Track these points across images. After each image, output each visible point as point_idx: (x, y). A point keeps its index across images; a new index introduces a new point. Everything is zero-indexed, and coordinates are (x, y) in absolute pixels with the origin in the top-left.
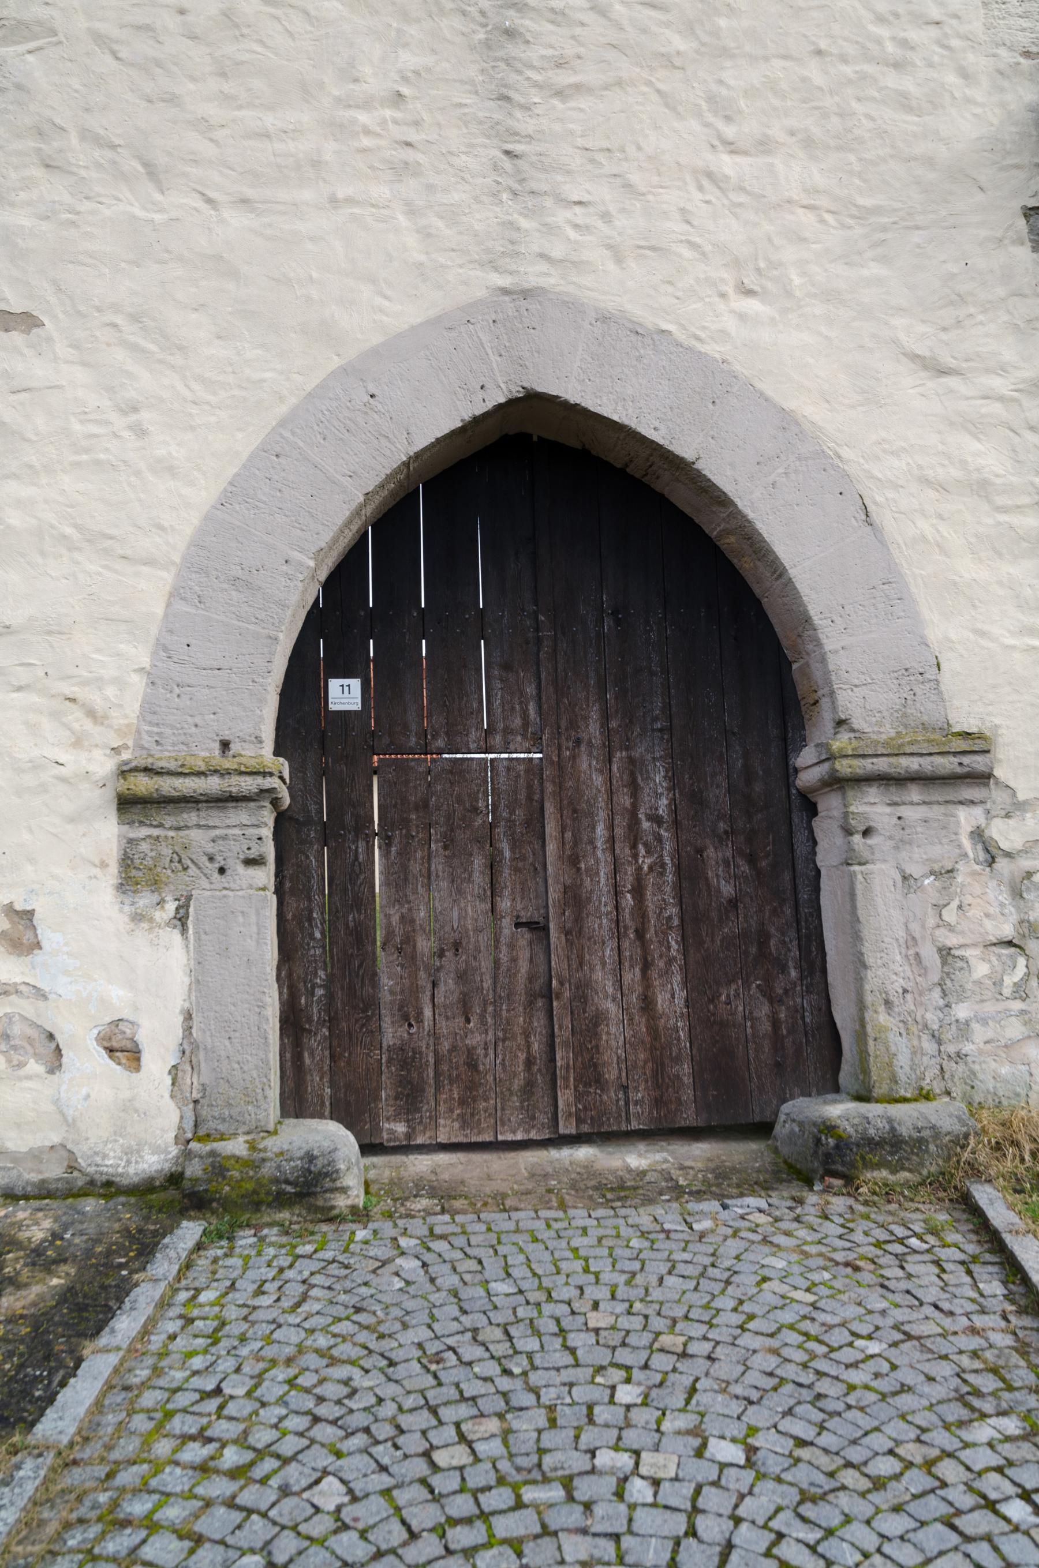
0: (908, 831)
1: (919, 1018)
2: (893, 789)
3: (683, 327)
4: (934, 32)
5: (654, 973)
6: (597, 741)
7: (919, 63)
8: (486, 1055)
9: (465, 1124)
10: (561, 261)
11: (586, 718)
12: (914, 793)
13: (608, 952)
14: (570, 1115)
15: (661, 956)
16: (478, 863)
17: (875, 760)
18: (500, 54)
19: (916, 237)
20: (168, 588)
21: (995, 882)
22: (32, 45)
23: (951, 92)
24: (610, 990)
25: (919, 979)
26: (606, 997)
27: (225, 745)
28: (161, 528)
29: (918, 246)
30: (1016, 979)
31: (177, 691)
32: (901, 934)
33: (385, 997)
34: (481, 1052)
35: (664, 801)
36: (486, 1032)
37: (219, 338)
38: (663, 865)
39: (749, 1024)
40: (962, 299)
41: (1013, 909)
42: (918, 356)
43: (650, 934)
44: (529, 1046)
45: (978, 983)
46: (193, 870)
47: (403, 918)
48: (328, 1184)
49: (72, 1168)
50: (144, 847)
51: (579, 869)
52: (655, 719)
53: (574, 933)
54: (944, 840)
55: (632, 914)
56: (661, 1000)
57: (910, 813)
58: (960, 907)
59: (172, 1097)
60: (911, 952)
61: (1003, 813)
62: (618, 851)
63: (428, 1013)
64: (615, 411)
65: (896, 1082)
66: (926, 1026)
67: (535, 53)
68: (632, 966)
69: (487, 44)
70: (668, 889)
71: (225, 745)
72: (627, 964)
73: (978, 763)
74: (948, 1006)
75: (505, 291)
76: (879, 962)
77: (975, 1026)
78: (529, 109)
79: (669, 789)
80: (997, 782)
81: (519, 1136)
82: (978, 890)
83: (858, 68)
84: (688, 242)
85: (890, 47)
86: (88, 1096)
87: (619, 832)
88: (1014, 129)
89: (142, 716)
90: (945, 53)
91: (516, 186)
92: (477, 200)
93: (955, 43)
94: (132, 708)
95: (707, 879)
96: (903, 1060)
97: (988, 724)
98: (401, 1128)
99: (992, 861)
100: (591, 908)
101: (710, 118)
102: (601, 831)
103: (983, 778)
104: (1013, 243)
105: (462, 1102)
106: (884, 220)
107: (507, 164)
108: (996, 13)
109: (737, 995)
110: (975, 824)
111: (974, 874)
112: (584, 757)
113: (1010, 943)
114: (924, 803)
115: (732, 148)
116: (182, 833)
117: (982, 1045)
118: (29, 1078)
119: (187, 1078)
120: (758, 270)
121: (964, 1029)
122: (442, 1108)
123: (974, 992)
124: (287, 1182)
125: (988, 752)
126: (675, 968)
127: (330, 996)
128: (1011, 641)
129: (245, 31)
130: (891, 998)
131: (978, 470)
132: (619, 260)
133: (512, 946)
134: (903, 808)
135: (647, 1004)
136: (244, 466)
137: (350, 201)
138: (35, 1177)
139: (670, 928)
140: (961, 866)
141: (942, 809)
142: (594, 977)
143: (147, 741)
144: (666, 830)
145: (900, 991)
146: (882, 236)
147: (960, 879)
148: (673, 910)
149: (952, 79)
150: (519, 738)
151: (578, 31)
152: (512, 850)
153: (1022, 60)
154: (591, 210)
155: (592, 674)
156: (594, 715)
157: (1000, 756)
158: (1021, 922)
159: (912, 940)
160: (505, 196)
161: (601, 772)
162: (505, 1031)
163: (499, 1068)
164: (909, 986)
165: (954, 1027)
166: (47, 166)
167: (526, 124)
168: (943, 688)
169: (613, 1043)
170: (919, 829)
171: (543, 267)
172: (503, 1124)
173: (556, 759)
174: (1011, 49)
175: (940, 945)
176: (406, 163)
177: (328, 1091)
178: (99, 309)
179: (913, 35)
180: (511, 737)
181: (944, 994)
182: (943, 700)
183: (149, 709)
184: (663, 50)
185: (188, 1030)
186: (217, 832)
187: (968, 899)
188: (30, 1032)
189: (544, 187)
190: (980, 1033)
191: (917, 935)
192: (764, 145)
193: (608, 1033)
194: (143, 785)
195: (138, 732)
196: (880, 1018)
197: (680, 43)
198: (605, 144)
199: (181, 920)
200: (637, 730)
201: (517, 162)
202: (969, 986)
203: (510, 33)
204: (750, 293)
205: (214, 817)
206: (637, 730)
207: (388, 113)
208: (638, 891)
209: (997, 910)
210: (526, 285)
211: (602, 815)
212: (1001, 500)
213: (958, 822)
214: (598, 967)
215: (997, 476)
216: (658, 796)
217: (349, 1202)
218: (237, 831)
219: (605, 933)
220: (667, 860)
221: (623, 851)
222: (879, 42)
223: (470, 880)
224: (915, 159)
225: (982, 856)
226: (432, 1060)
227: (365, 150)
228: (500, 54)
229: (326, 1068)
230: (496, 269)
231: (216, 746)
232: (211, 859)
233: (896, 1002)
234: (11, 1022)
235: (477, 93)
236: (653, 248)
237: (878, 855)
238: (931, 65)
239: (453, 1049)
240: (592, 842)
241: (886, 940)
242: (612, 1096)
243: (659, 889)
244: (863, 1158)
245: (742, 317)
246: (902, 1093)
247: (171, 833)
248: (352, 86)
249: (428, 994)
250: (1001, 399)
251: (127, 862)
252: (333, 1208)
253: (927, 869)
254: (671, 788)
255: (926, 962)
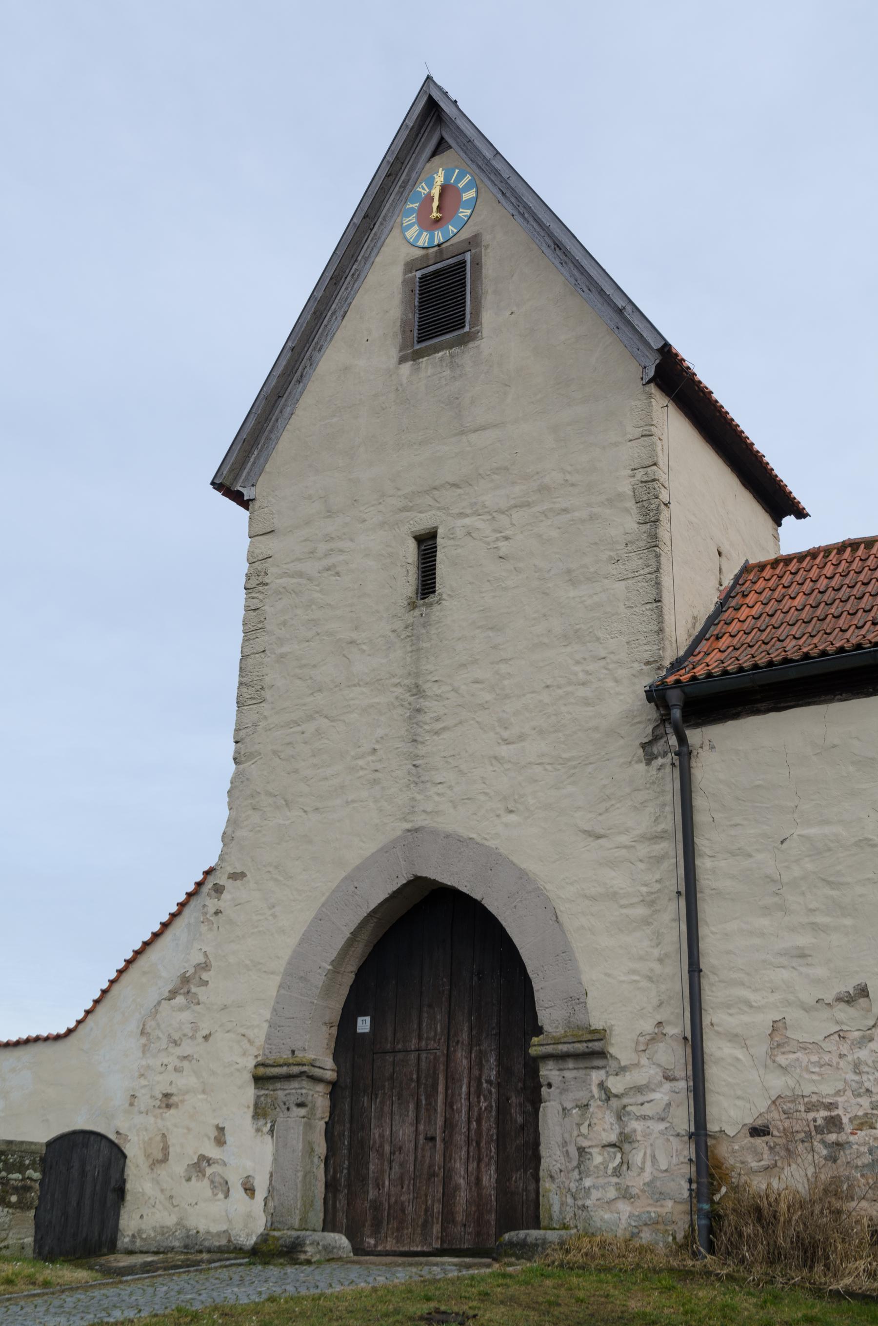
0: (567, 1084)
1: (566, 1185)
2: (560, 1062)
3: (479, 834)
4: (602, 663)
5: (483, 1165)
6: (466, 1042)
7: (594, 681)
8: (409, 1206)
9: (398, 1240)
10: (431, 812)
11: (462, 1030)
12: (571, 1064)
13: (463, 1153)
14: (438, 1238)
15: (487, 1156)
16: (412, 1106)
17: (547, 1047)
18: (414, 721)
19: (590, 769)
20: (278, 984)
21: (609, 1112)
22: (252, 762)
23: (609, 691)
24: (462, 1173)
25: (568, 1164)
26: (460, 1176)
27: (293, 1052)
28: (278, 958)
29: (590, 773)
30: (615, 1165)
31: (278, 1029)
32: (559, 1139)
33: (371, 1175)
34: (407, 1204)
35: (494, 1072)
36: (410, 1194)
37: (304, 870)
38: (491, 1107)
39: (525, 1193)
40: (609, 798)
41: (617, 1127)
42: (586, 831)
43: (483, 1144)
44: (427, 1201)
45: (596, 1167)
46: (278, 1109)
47: (380, 1135)
48: (299, 1249)
49: (229, 1241)
50: (262, 1099)
51: (453, 1109)
52: (493, 1029)
53: (448, 1143)
54: (584, 1089)
55: (475, 1133)
56: (485, 1179)
57: (568, 1074)
58: (589, 1125)
59: (264, 1211)
60: (565, 1149)
61: (615, 1073)
62: (471, 1099)
63: (387, 1183)
64: (449, 880)
65: (552, 1220)
66: (569, 1190)
67: (426, 718)
68: (473, 1161)
69: (410, 718)
70: (492, 1119)
71: (293, 1052)
72: (471, 1160)
73: (596, 1046)
74: (581, 1179)
75: (409, 831)
76: (548, 1154)
77: (593, 1191)
78: (424, 743)
79: (496, 1066)
80: (611, 1056)
81: (419, 1249)
82: (600, 1115)
83: (565, 690)
84: (484, 793)
85: (581, 676)
86: (236, 1210)
87: (472, 1089)
88: (639, 703)
89: (266, 1041)
90: (607, 672)
91: (416, 780)
92: (401, 790)
93: (611, 666)
94: (263, 1038)
95: (511, 1114)
96: (556, 1208)
97: (608, 1025)
98: (372, 1241)
99: (608, 1099)
100: (457, 1130)
101: (498, 729)
102: (464, 1089)
103: (602, 1054)
104: (637, 762)
105: (398, 1230)
106: (574, 763)
107: (414, 770)
108: (633, 646)
109: (520, 1178)
110: (600, 1079)
111: (599, 1107)
112: (460, 1051)
113: (614, 1145)
114: (575, 1069)
115: (507, 742)
116: (275, 1092)
117: (595, 1201)
118: (219, 1200)
119: (271, 1204)
120: (515, 800)
121: (588, 1191)
122: (389, 1232)
123: (594, 1172)
124: (286, 1247)
125: (602, 1040)
126: (493, 1162)
127: (349, 1173)
128: (623, 978)
129: (323, 735)
130: (553, 1174)
131: (611, 887)
132: (455, 807)
133: (423, 1149)
134: (565, 1072)
135: (478, 1180)
136: (308, 927)
137: (353, 801)
138: (217, 1244)
139: (492, 1140)
140: (591, 1102)
141: (584, 1072)
142: (456, 1166)
143: (267, 1052)
144: (494, 1088)
145: (558, 1171)
146: (572, 771)
147: (591, 1110)
148: (494, 1131)
149: (610, 684)
150: (432, 1042)
151: (446, 702)
152: (426, 1100)
153: (644, 667)
154: (445, 785)
155: (466, 1007)
156: (466, 1029)
157: (613, 1041)
158: (621, 1133)
159: (565, 1143)
160: (412, 786)
161: (466, 1058)
162: (417, 1194)
163: (414, 1212)
164: (563, 1168)
165: (583, 1191)
166: (254, 809)
167: (422, 750)
168: (588, 1006)
169: (462, 1201)
170: (572, 1083)
171: (424, 816)
172: (413, 1242)
173: (445, 1052)
174: (639, 662)
175: (579, 1146)
176: (375, 780)
177: (345, 1220)
178: (264, 866)
179: (591, 667)
180: (429, 1042)
181: (580, 1173)
182: (588, 1013)
183: (268, 1038)
184: (480, 702)
185: (271, 1181)
186: (287, 1092)
187: (595, 1121)
188: (221, 1181)
189: (427, 778)
190: (595, 1194)
191: (568, 1140)
192: (522, 737)
193: (460, 1196)
194: (261, 1071)
195: (264, 1048)
196: (546, 1184)
197: (489, 697)
198: (452, 753)
199: (272, 1131)
200: (484, 1035)
201: (418, 769)
202: (592, 1168)
203: (419, 711)
204: (511, 812)
205: (286, 1085)
206: (484, 1035)
207: (370, 758)
208: (479, 1121)
209: (609, 1127)
210: (417, 826)
211: (465, 1080)
212: (623, 902)
213: (591, 1079)
214: (458, 1161)
215: (621, 889)
216: (491, 1069)
217: (306, 1257)
218: (294, 1091)
219: (463, 1143)
220: (493, 1104)
221: (473, 1099)
222: (576, 674)
223: (407, 1116)
224: (590, 729)
225: (604, 1097)
226: (387, 1208)
227: (360, 777)
228: (414, 721)
229: (345, 1209)
230: (406, 821)
231: (290, 1052)
232: (285, 1104)
233: (556, 1176)
234: (215, 1176)
235: (404, 741)
236: (468, 799)
237: (552, 1097)
238: (600, 680)
239: (396, 1202)
240: (460, 1095)
241: (552, 1142)
242: (458, 1230)
243: (488, 1119)
244: (505, 1251)
245: (506, 825)
246: (555, 1226)
247: (272, 1093)
248: (358, 750)
249: (388, 1173)
250: (625, 847)
251: (256, 1106)
252: (298, 1259)
253: (574, 1104)
254: (498, 1065)
255: (571, 1155)
